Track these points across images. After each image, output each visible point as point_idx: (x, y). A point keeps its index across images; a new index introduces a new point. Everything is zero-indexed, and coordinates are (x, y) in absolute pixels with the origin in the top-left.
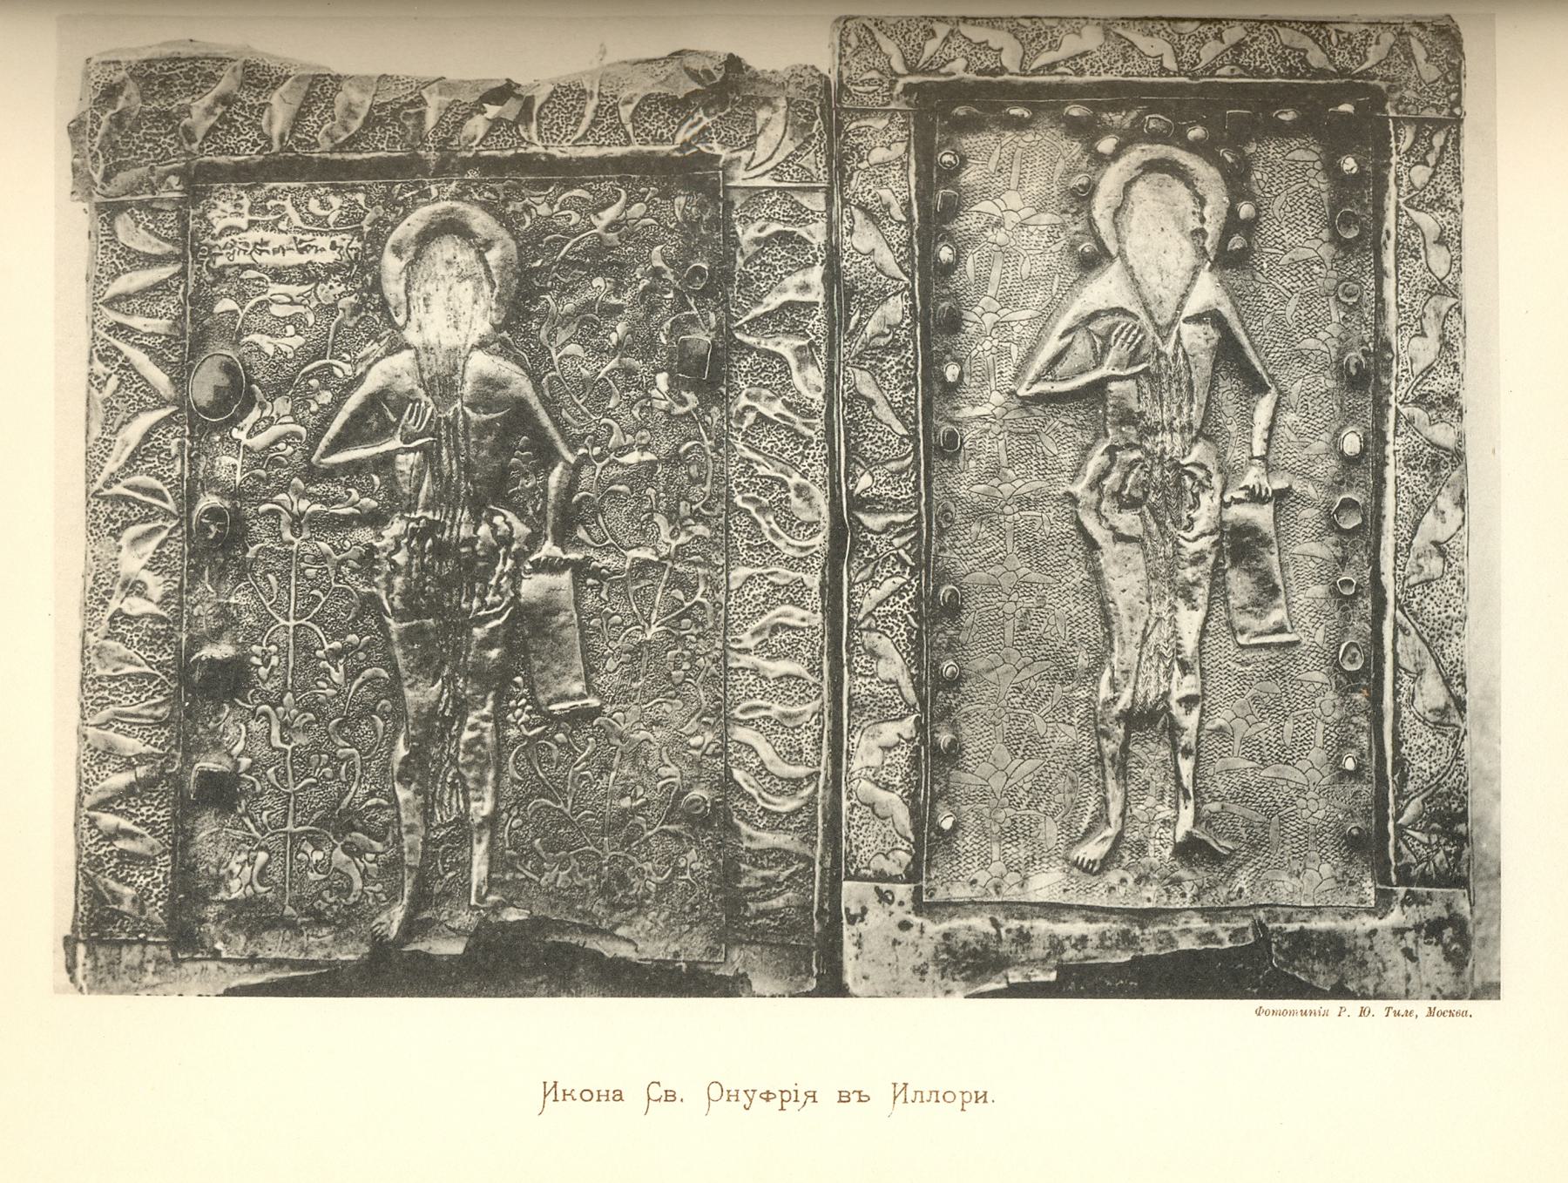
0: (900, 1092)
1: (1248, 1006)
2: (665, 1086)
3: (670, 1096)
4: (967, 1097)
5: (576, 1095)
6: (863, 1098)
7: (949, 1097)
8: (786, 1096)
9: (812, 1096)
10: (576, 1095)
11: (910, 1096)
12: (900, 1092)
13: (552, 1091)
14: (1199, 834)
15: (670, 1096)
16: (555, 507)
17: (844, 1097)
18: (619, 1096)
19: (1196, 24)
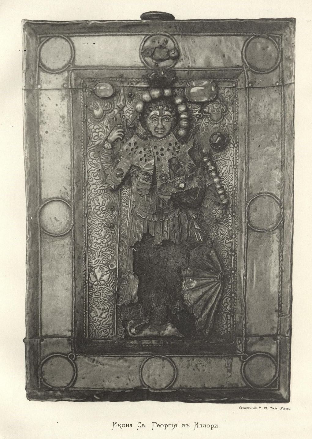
0: (196, 424)
2: (142, 423)
3: (143, 426)
6: (188, 426)
8: (166, 426)
12: (196, 424)
15: (143, 426)
17: (183, 426)
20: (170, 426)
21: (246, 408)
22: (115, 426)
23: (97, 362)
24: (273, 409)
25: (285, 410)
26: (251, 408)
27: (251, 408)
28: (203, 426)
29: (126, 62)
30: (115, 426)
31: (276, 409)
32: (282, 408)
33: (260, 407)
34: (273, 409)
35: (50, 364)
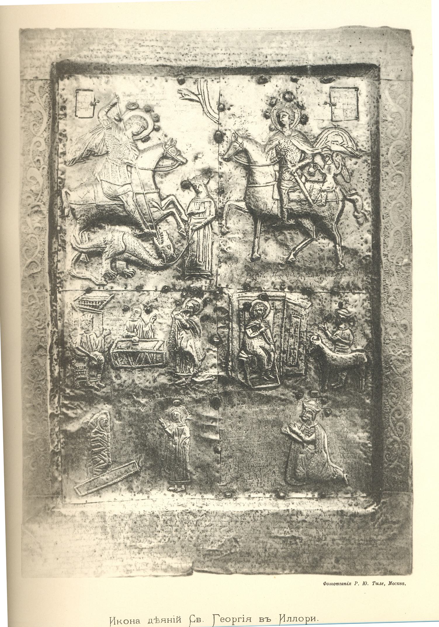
0: (282, 617)
1: (242, 76)
2: (197, 616)
3: (198, 620)
4: (308, 619)
5: (122, 622)
6: (268, 620)
7: (301, 619)
8: (308, 619)
9: (179, 620)
10: (122, 622)
11: (286, 619)
12: (282, 617)
13: (113, 621)
14: (200, 316)
15: (198, 620)
16: (279, 494)
17: (261, 620)
18: (179, 620)
19: (80, 275)
20: (241, 620)
21: (334, 584)
22: (283, 619)
23: (261, 334)
24: (377, 584)
25: (396, 586)
26: (342, 584)
27: (342, 584)
28: (292, 619)
29: (64, 154)
30: (283, 619)
31: (382, 584)
32: (390, 583)
33: (356, 582)
34: (377, 584)
35: (156, 303)
